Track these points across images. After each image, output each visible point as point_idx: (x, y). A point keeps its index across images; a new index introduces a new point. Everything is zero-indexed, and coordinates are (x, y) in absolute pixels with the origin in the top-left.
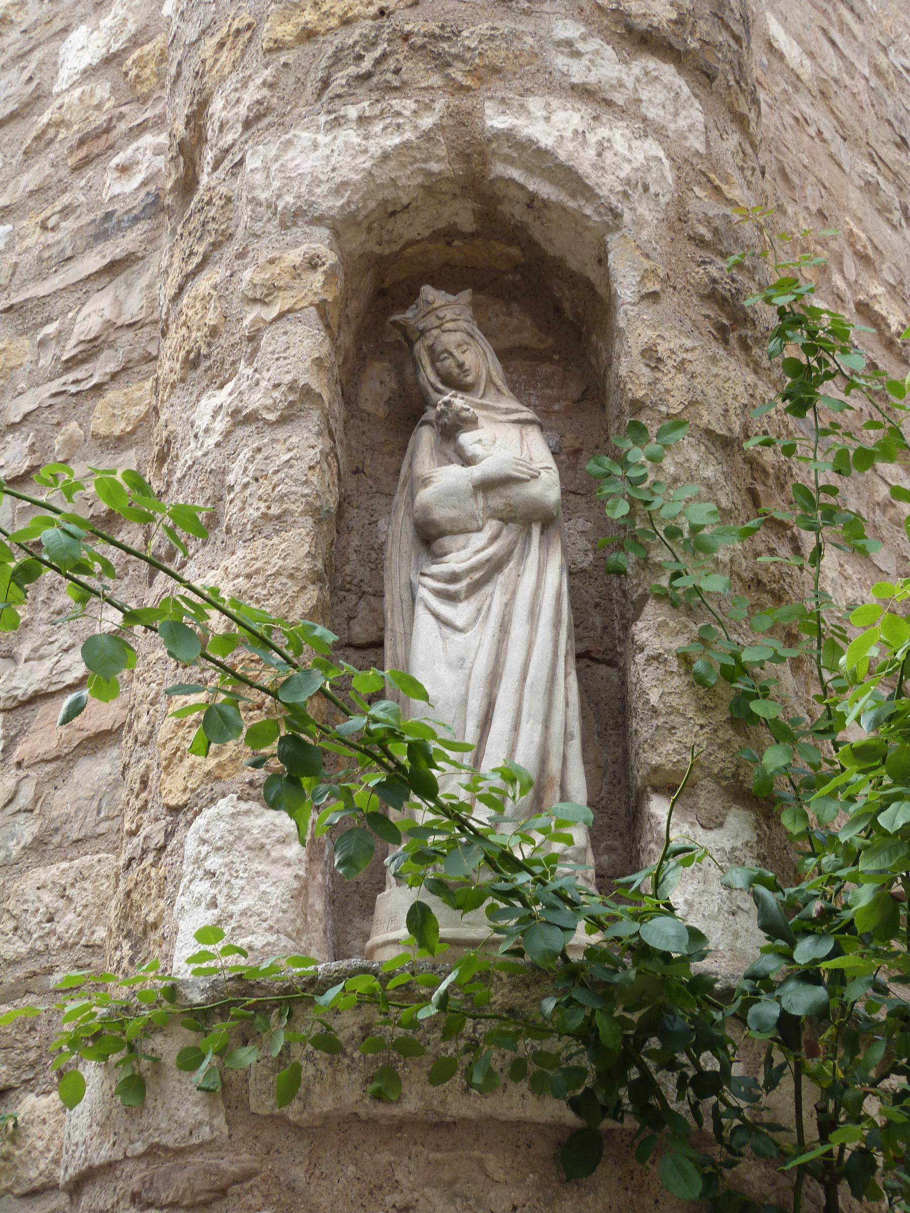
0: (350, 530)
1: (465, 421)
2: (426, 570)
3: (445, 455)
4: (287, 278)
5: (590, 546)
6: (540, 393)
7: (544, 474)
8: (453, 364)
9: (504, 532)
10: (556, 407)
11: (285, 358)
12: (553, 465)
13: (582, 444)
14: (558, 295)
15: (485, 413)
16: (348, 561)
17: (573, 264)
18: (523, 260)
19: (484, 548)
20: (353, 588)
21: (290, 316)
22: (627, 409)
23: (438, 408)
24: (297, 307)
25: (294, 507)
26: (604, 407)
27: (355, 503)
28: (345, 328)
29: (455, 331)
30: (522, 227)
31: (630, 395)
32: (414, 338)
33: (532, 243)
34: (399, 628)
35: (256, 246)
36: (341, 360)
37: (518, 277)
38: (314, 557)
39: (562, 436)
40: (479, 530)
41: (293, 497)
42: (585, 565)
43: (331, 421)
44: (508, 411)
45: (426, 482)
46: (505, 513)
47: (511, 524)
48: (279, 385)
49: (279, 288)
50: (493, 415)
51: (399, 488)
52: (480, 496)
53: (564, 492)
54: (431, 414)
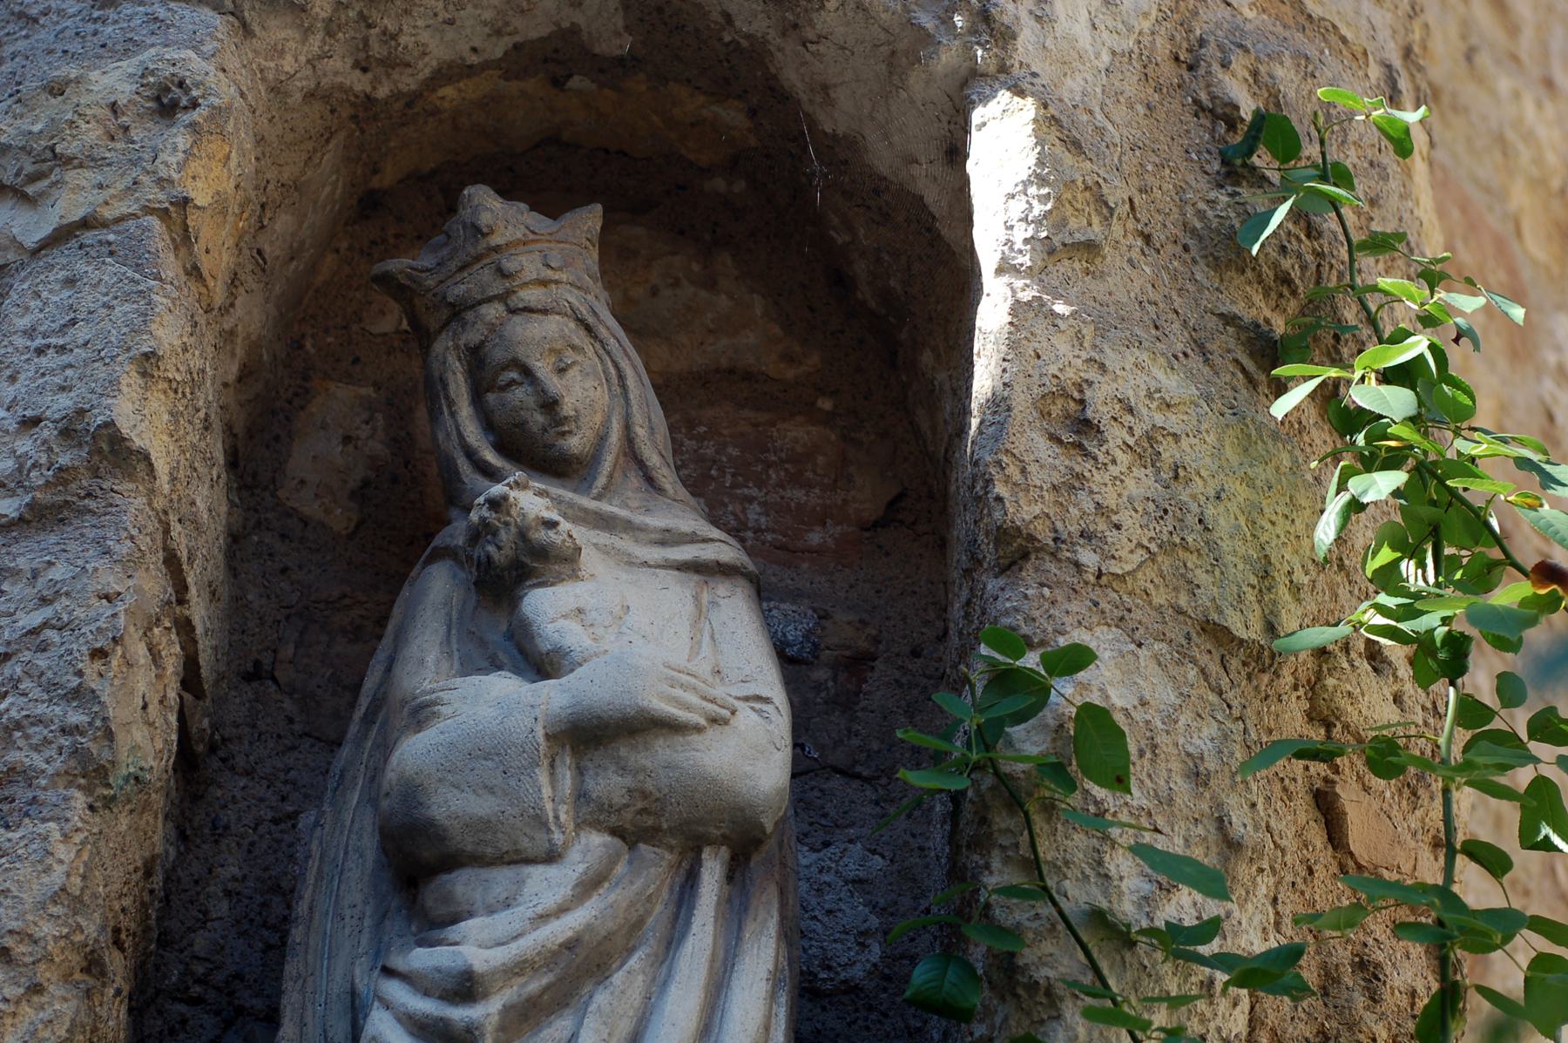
0: (219, 831)
1: (543, 553)
2: (398, 962)
3: (483, 643)
4: (91, 134)
5: (874, 922)
6: (774, 498)
7: (746, 718)
8: (531, 401)
9: (620, 869)
10: (815, 538)
11: (62, 349)
12: (778, 695)
13: (876, 641)
14: (841, 239)
15: (603, 538)
16: (205, 918)
17: (882, 159)
18: (753, 142)
19: (562, 910)
20: (211, 995)
21: (89, 237)
22: (988, 551)
23: (474, 516)
24: (107, 214)
25: (38, 760)
26: (943, 544)
27: (240, 761)
28: (251, 282)
29: (545, 312)
30: (756, 53)
31: (997, 515)
32: (433, 323)
33: (777, 94)
34: (781, 959)
35: (21, 45)
36: (234, 369)
37: (740, 186)
38: (77, 904)
39: (824, 616)
40: (551, 857)
41: (38, 732)
42: (857, 972)
43: (176, 529)
44: (668, 538)
45: (421, 714)
46: (628, 815)
47: (643, 847)
48: (35, 422)
49: (67, 161)
50: (625, 543)
51: (353, 729)
52: (566, 763)
53: (797, 773)
54: (455, 534)
